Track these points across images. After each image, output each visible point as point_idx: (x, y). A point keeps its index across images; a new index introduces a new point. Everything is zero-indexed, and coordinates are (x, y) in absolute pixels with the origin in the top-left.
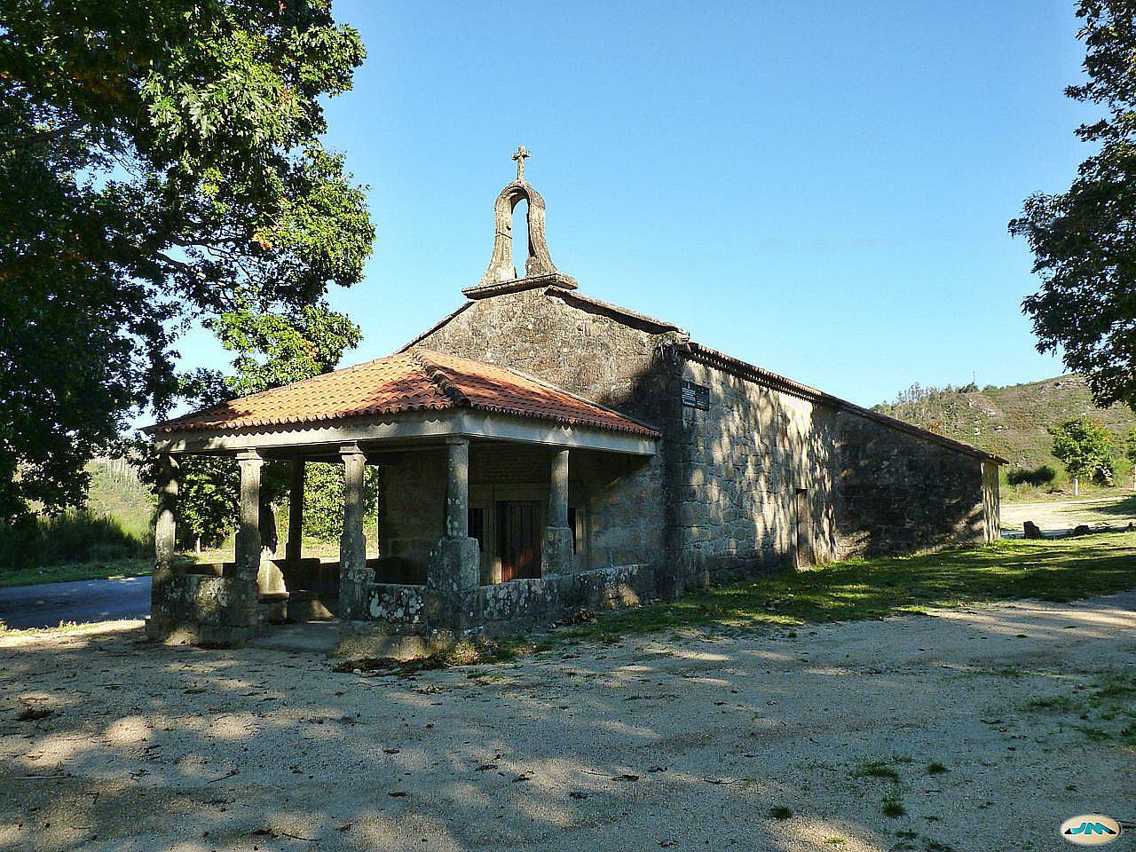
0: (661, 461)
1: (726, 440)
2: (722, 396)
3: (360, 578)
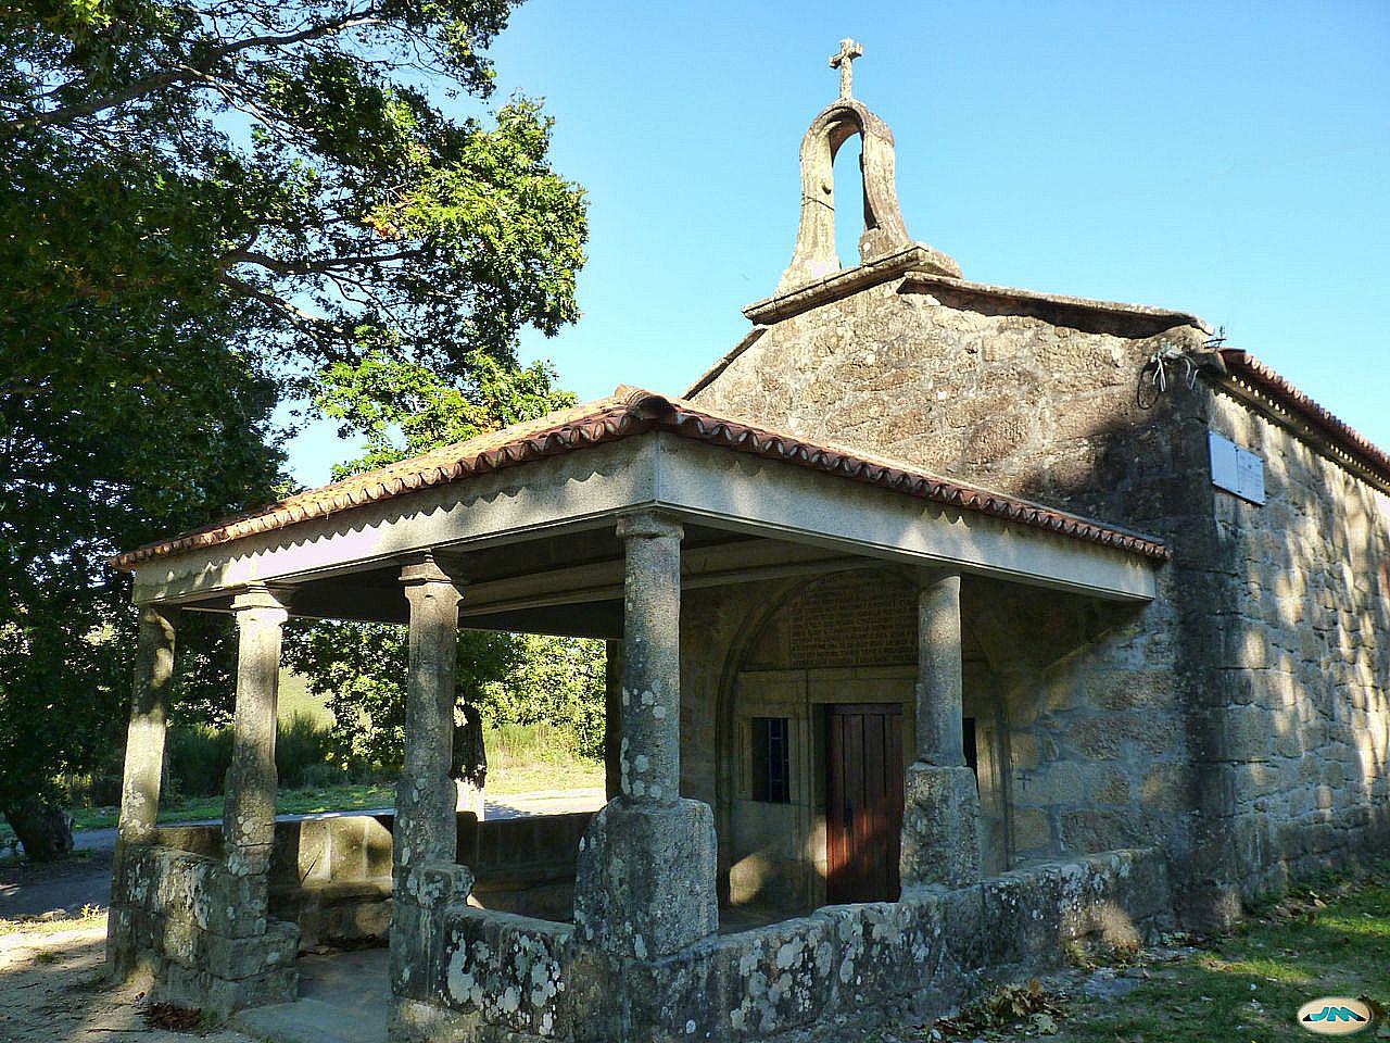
0: (1170, 613)
1: (1297, 574)
2: (1285, 480)
3: (429, 893)
